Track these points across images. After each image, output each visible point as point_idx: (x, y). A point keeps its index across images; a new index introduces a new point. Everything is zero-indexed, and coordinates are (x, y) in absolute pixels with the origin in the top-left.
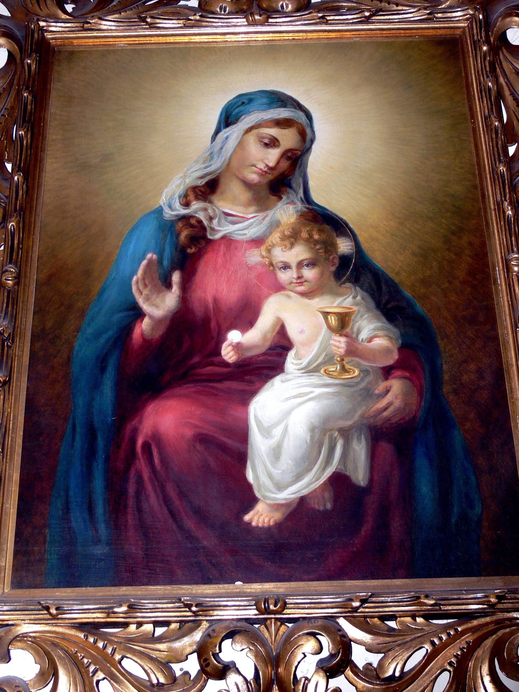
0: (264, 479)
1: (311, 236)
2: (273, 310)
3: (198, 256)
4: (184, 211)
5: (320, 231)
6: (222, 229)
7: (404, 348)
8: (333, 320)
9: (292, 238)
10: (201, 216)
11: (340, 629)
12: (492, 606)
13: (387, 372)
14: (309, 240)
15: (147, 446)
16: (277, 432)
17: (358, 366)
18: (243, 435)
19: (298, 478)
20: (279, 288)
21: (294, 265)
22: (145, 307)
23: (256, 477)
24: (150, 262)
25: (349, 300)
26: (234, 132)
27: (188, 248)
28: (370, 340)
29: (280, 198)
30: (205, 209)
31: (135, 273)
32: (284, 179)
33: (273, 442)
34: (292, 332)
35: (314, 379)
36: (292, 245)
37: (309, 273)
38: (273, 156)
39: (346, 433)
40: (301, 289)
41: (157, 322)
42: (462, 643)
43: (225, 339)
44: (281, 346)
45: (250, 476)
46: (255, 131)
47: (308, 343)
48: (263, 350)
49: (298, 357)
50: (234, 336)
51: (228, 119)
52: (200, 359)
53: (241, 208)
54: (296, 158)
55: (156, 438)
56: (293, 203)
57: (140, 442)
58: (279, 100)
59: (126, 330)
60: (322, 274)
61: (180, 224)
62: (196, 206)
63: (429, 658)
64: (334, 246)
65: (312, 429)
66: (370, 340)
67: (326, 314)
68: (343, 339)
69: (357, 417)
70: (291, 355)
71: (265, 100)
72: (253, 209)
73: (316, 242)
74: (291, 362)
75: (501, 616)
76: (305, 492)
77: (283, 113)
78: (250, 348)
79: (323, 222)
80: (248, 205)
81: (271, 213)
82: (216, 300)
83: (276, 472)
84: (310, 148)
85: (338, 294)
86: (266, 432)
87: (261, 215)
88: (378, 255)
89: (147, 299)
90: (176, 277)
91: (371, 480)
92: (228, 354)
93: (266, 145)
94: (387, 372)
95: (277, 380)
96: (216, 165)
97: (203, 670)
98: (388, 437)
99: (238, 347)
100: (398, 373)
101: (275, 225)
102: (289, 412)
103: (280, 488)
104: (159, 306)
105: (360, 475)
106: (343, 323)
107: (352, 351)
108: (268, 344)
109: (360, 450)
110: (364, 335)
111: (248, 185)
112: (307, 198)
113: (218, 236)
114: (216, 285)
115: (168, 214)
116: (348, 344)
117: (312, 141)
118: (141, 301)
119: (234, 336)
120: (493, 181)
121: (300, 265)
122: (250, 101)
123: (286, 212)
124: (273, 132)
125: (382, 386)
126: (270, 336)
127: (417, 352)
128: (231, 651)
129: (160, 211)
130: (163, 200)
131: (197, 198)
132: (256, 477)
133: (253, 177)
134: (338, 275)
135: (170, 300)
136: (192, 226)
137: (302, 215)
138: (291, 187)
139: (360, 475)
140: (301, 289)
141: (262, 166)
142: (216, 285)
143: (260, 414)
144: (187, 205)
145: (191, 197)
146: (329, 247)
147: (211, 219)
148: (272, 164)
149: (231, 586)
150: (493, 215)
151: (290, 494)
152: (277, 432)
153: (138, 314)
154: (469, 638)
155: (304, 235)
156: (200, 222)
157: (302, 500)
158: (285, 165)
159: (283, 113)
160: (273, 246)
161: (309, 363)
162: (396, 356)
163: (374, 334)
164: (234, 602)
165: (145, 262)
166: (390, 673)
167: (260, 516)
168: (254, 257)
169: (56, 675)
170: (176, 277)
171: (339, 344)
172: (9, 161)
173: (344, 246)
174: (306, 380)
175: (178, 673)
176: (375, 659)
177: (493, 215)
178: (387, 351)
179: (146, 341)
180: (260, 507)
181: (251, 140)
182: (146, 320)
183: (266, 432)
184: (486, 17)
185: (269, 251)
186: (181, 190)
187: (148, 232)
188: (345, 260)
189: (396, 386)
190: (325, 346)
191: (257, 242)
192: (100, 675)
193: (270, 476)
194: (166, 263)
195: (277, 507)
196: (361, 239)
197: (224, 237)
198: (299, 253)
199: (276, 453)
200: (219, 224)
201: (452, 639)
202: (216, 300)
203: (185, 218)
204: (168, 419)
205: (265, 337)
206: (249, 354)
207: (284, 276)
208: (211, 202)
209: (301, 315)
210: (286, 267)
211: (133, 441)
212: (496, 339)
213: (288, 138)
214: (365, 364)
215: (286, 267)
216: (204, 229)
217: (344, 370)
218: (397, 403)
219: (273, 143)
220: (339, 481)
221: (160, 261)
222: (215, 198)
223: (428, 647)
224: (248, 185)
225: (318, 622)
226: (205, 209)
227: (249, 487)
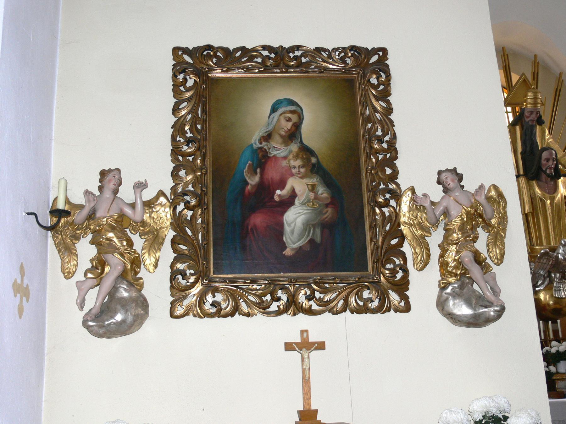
0: (289, 240)
1: (303, 156)
2: (291, 183)
3: (265, 163)
4: (260, 146)
5: (306, 155)
6: (273, 153)
7: (332, 198)
8: (310, 187)
9: (296, 157)
10: (266, 147)
11: (312, 287)
12: (356, 281)
13: (327, 206)
14: (302, 158)
15: (252, 229)
16: (293, 225)
17: (318, 203)
18: (282, 225)
19: (299, 240)
20: (292, 175)
21: (297, 167)
22: (249, 181)
23: (286, 240)
24: (250, 164)
25: (314, 180)
26: (276, 115)
27: (262, 159)
28: (322, 194)
29: (292, 142)
30: (267, 145)
31: (245, 168)
32: (294, 134)
33: (291, 228)
34: (297, 191)
35: (304, 208)
36: (296, 160)
37: (302, 170)
38: (289, 125)
39: (314, 226)
40: (299, 175)
41: (253, 186)
42: (347, 291)
43: (275, 193)
44: (293, 195)
45: (285, 240)
46: (283, 115)
47: (303, 194)
48: (287, 197)
49: (299, 200)
50: (278, 192)
51: (274, 109)
52: (268, 201)
53: (279, 145)
54: (297, 126)
55: (255, 226)
56: (296, 143)
57: (250, 228)
58: (291, 102)
59: (243, 189)
60: (306, 170)
61: (259, 151)
62: (264, 143)
63: (338, 295)
64: (310, 160)
65: (303, 224)
66: (322, 194)
67: (308, 185)
68: (313, 194)
69: (317, 221)
70: (297, 199)
71: (286, 103)
72: (283, 145)
73: (304, 159)
74: (297, 202)
75: (359, 283)
76: (301, 245)
77: (293, 108)
78: (284, 196)
79: (306, 151)
80: (281, 144)
81: (289, 147)
82: (272, 179)
83: (292, 238)
84: (506, 212)
85: (312, 178)
86: (289, 225)
87: (286, 148)
88: (325, 164)
89: (249, 178)
90: (258, 170)
91: (322, 241)
92: (276, 198)
93: (287, 121)
94: (327, 206)
95: (292, 207)
96: (270, 128)
97: (272, 299)
98: (326, 226)
99: (279, 196)
100: (330, 206)
101: (291, 152)
102: (297, 218)
103: (294, 243)
104: (253, 180)
105: (318, 240)
106: (313, 188)
107: (316, 198)
108: (289, 195)
109: (318, 231)
110: (320, 192)
111: (281, 136)
112: (301, 142)
113: (272, 155)
114: (272, 174)
115: (255, 146)
116: (315, 196)
117: (303, 119)
118: (247, 179)
119: (278, 192)
120: (363, 139)
121: (299, 167)
122: (281, 102)
123: (294, 147)
124: (289, 115)
125: (326, 210)
126: (290, 192)
127: (336, 200)
128: (279, 293)
129: (252, 145)
130: (253, 141)
131: (264, 141)
132: (286, 240)
133: (283, 133)
134: (312, 171)
135: (257, 179)
136: (263, 151)
137: (300, 148)
138: (295, 137)
139: (318, 240)
140: (299, 175)
141: (286, 129)
142: (272, 174)
143: (287, 219)
144: (261, 143)
145: (262, 140)
146: (309, 160)
147: (269, 149)
148: (289, 128)
149: (280, 274)
150: (362, 151)
151: (296, 245)
152: (293, 225)
153: (247, 184)
154: (349, 290)
155: (300, 156)
156: (266, 150)
157: (301, 247)
158: (294, 128)
159: (293, 108)
160: (290, 159)
161: (303, 202)
162: (330, 200)
163: (322, 192)
164: (284, 276)
165: (248, 165)
166: (326, 300)
167: (288, 252)
168: (284, 163)
169: (229, 299)
170: (258, 170)
171: (312, 195)
172: (199, 124)
173: (314, 160)
174: (301, 208)
175: (264, 300)
176: (322, 296)
177: (362, 151)
178: (326, 198)
179: (249, 193)
180: (288, 249)
181: (282, 118)
182: (249, 186)
183: (289, 225)
184: (364, 73)
185: (289, 161)
186: (258, 138)
187: (248, 153)
188: (314, 165)
189: (330, 210)
190: (307, 196)
191: (285, 158)
192: (242, 300)
193: (291, 240)
194: (255, 165)
195: (293, 249)
196: (319, 157)
197: (274, 156)
198: (298, 163)
199: (292, 232)
200: (272, 151)
201: (346, 289)
202: (272, 179)
203: (261, 148)
204: (258, 220)
205: (288, 192)
206: (283, 198)
207: (294, 171)
208: (269, 142)
209: (298, 184)
210: (295, 167)
211: (247, 228)
212: (362, 194)
213: (294, 118)
214: (320, 202)
215: (295, 167)
216: (267, 153)
217: (313, 205)
218: (330, 216)
219: (289, 120)
220: (312, 242)
221: (253, 164)
222: (270, 141)
223: (337, 293)
224: (281, 136)
225: (278, 306)
226: (267, 145)
227: (284, 243)
